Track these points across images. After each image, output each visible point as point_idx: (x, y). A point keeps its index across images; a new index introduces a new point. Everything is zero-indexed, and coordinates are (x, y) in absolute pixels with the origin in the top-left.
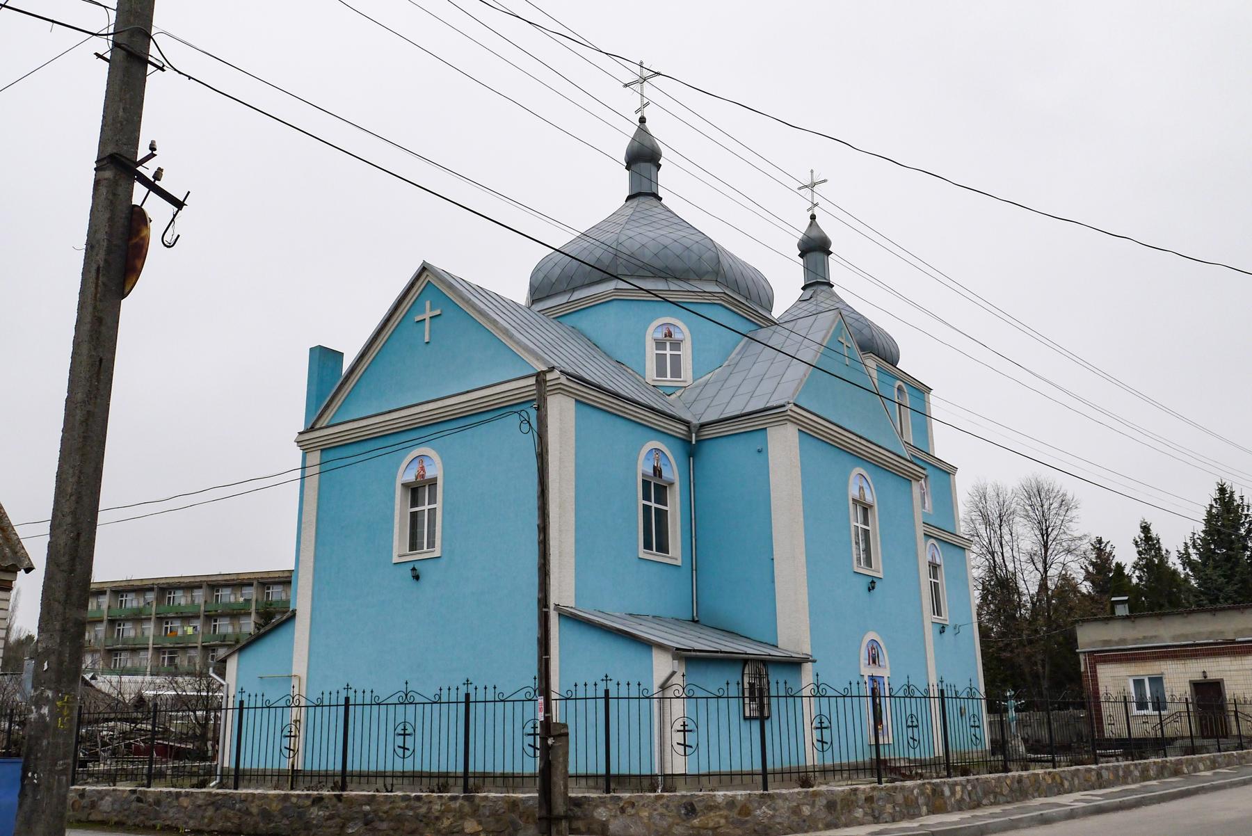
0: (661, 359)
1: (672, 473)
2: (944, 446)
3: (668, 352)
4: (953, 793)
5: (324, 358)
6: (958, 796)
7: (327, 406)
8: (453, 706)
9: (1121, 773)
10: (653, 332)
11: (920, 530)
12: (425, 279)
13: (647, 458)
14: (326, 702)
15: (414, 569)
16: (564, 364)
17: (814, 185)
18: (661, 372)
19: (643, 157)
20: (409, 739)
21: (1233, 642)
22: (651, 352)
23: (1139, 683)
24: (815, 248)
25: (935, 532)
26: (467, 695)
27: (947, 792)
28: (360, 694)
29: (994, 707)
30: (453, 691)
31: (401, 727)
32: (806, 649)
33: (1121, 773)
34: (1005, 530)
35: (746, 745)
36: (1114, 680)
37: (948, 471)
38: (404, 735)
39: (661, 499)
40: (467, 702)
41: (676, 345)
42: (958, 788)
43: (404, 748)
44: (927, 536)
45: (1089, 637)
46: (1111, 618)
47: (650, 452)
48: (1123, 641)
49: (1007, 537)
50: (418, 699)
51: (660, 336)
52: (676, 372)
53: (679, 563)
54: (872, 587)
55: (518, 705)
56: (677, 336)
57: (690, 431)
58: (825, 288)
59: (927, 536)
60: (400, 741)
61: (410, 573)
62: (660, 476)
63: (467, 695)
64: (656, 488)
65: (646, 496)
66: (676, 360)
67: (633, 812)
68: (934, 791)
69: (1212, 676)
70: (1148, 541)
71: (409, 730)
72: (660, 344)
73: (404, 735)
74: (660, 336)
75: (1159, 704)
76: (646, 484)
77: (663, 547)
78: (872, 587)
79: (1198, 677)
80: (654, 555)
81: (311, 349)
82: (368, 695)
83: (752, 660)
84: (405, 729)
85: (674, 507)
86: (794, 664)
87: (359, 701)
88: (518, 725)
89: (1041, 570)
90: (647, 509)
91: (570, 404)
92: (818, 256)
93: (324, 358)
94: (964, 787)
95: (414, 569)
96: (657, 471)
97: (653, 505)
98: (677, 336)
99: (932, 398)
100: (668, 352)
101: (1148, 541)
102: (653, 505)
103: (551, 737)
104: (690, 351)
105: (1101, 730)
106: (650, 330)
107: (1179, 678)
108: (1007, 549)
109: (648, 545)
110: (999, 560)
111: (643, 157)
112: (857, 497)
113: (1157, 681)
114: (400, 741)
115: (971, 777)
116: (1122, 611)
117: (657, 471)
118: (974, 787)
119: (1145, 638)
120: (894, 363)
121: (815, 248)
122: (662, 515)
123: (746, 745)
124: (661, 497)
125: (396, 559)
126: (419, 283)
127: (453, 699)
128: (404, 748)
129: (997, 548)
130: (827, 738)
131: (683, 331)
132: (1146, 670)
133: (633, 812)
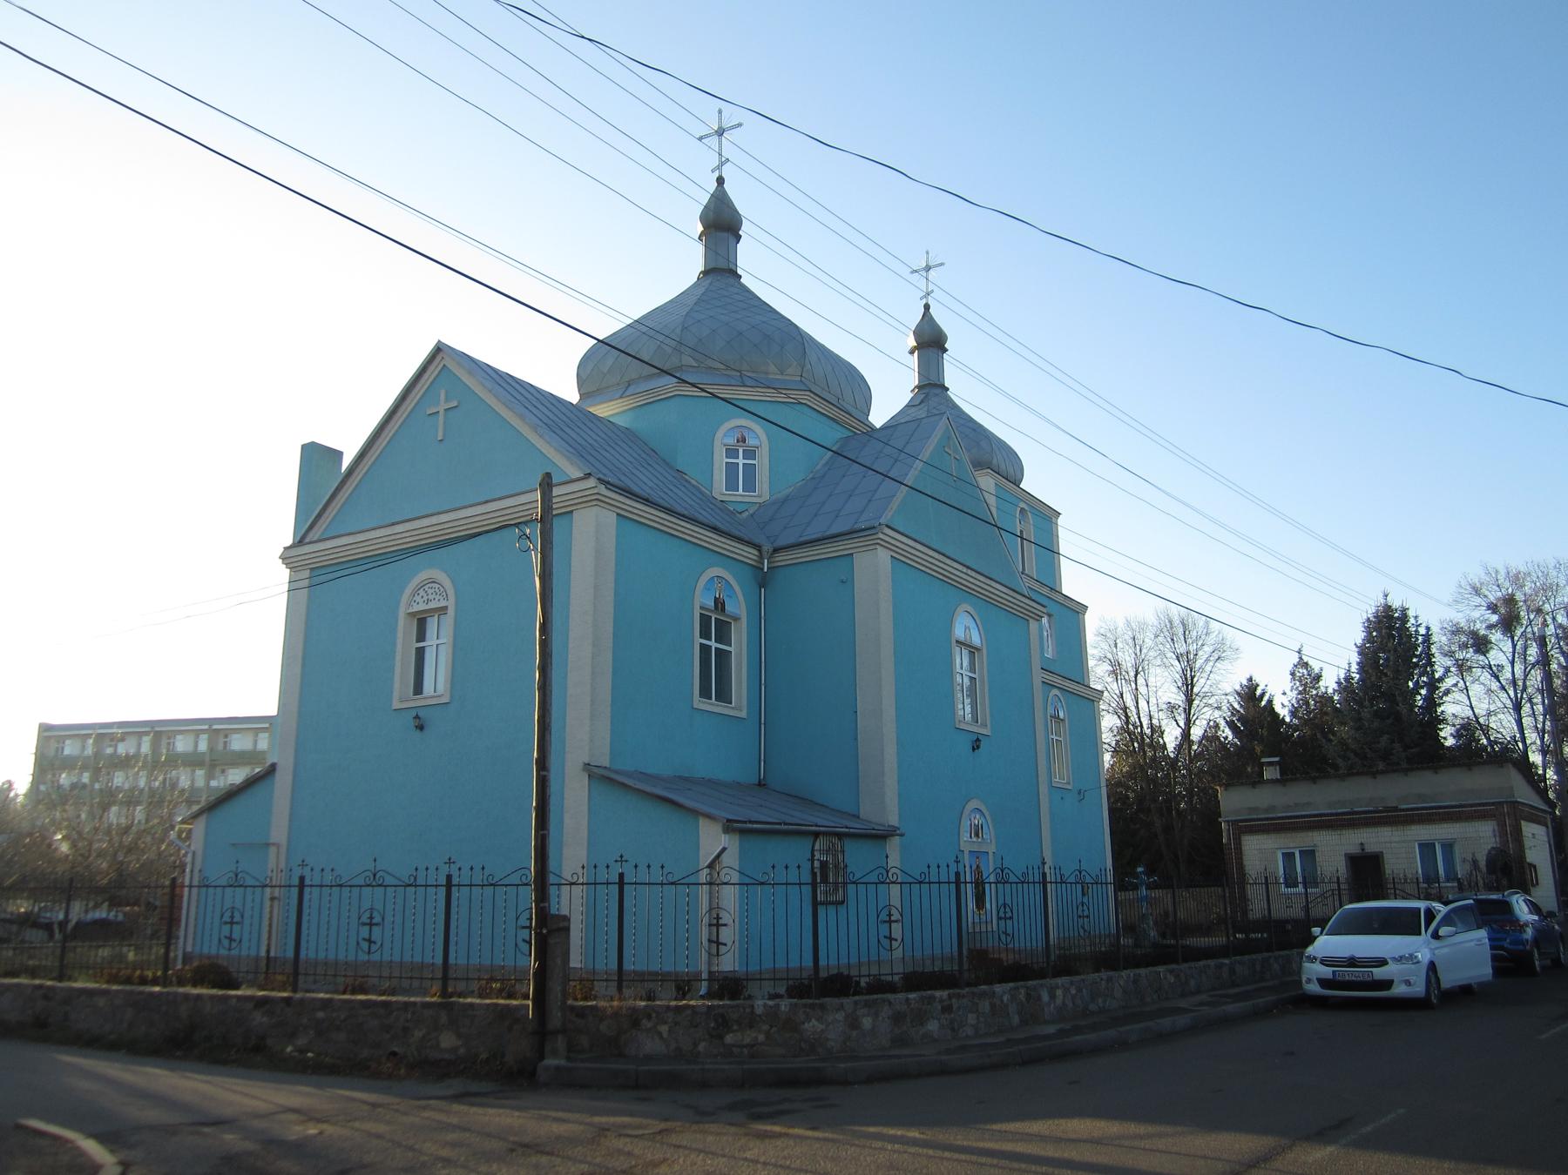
0: (732, 469)
1: (737, 606)
2: (1073, 583)
3: (741, 461)
4: (1053, 997)
5: (316, 457)
6: (1059, 1001)
7: (319, 516)
8: (431, 890)
9: (1258, 968)
10: (724, 436)
11: (1038, 677)
12: (442, 363)
13: (707, 588)
14: (420, 881)
15: (417, 717)
16: (605, 471)
17: (928, 268)
18: (731, 484)
19: (721, 224)
20: (236, 928)
21: (1396, 809)
22: (721, 460)
23: (1289, 857)
24: (931, 342)
25: (1058, 681)
26: (449, 877)
27: (1045, 997)
28: (466, 872)
29: (1121, 885)
30: (943, 869)
31: (367, 915)
32: (893, 820)
33: (1258, 968)
34: (1141, 680)
35: (833, 930)
36: (1261, 854)
37: (1077, 610)
38: (371, 925)
39: (723, 636)
40: (449, 885)
41: (750, 454)
42: (1059, 992)
43: (370, 941)
44: (1048, 685)
45: (1233, 802)
46: (1257, 781)
47: (715, 578)
48: (1272, 808)
49: (1142, 689)
50: (389, 880)
51: (731, 441)
52: (750, 485)
53: (743, 714)
54: (976, 745)
55: (872, 888)
56: (751, 441)
57: (761, 557)
58: (938, 391)
59: (1048, 685)
60: (365, 931)
61: (412, 723)
62: (723, 609)
63: (449, 877)
64: (716, 624)
65: (705, 633)
66: (750, 471)
67: (649, 1025)
68: (1028, 996)
69: (1371, 848)
70: (1306, 676)
71: (237, 918)
72: (731, 452)
73: (371, 925)
74: (731, 441)
75: (1310, 880)
76: (705, 621)
77: (724, 695)
78: (976, 745)
79: (1355, 850)
80: (713, 706)
81: (304, 447)
82: (655, 869)
83: (825, 834)
84: (371, 918)
85: (739, 646)
86: (881, 836)
87: (317, 881)
88: (218, 914)
89: (1182, 724)
90: (705, 650)
91: (610, 518)
92: (932, 352)
93: (316, 457)
94: (1066, 990)
95: (417, 717)
96: (719, 605)
97: (713, 644)
98: (751, 441)
99: (1060, 521)
100: (741, 461)
101: (1306, 676)
102: (713, 644)
103: (549, 931)
104: (766, 461)
105: (1245, 912)
106: (719, 435)
107: (1333, 851)
108: (1142, 704)
109: (705, 693)
110: (1134, 718)
111: (721, 224)
112: (962, 638)
113: (1309, 855)
114: (226, 929)
115: (1078, 978)
116: (1269, 774)
117: (719, 605)
118: (1079, 990)
119: (1296, 805)
120: (1017, 482)
121: (931, 342)
122: (723, 656)
123: (833, 930)
124: (723, 634)
125: (397, 705)
126: (432, 368)
127: (944, 878)
128: (370, 941)
129: (1130, 703)
130: (236, 935)
131: (759, 435)
132: (1296, 842)
133: (649, 1025)
